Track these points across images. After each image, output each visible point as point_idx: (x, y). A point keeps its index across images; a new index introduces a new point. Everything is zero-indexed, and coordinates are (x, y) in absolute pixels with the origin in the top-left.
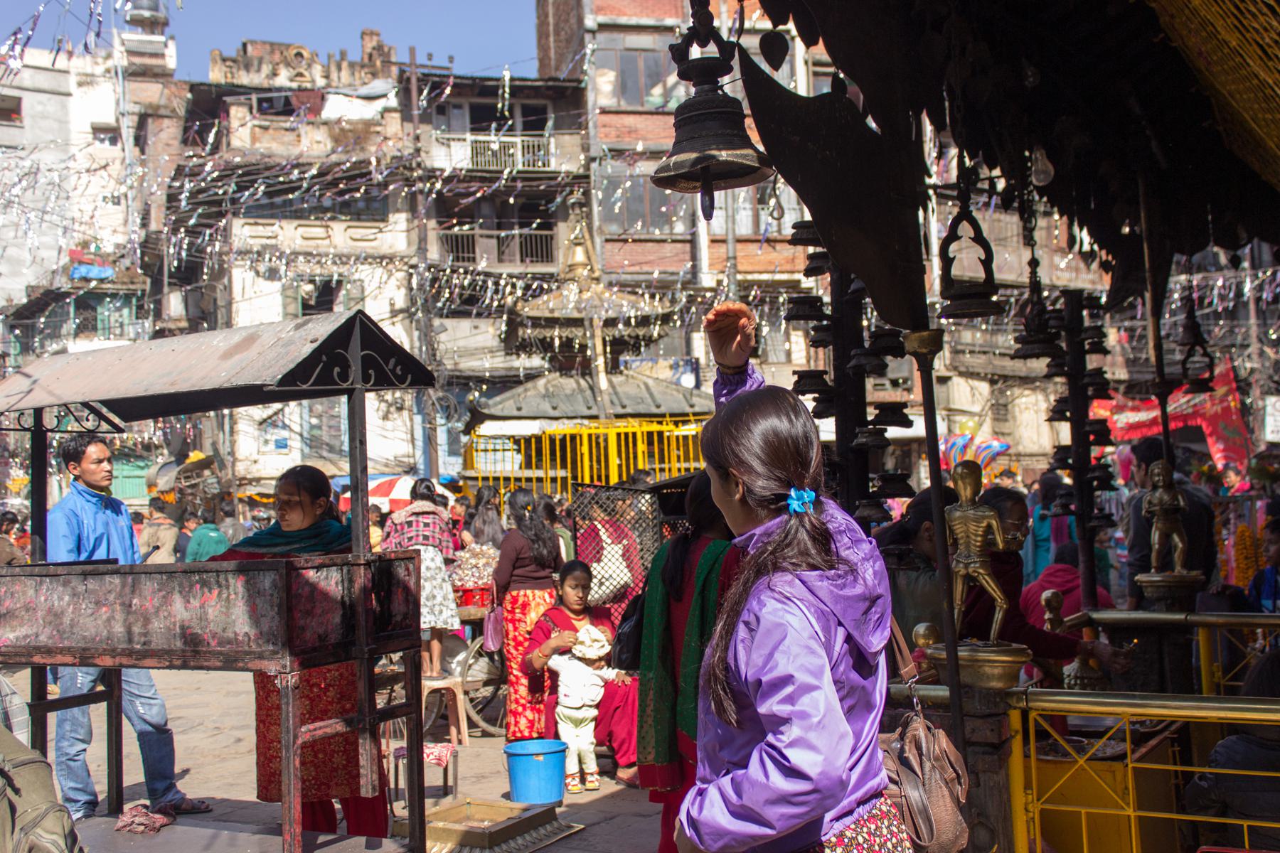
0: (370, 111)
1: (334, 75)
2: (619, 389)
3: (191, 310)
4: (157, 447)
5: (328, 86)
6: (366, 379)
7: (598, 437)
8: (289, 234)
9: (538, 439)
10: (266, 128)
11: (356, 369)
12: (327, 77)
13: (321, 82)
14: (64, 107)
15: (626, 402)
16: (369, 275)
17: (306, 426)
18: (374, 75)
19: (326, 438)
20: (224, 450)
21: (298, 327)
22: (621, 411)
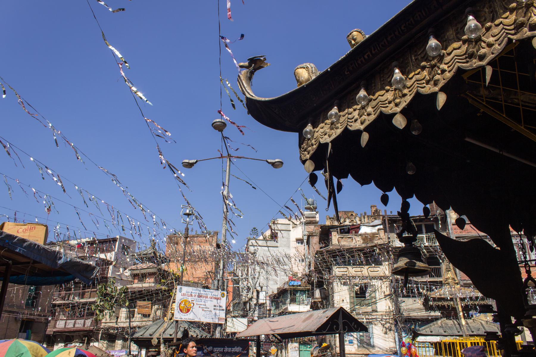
0: (375, 230)
1: (363, 220)
2: (470, 325)
3: (322, 296)
4: (314, 341)
5: (361, 223)
6: (344, 329)
7: (463, 343)
8: (352, 271)
9: (440, 343)
10: (343, 238)
11: (341, 326)
12: (360, 221)
13: (359, 222)
14: (289, 234)
15: (473, 330)
16: (376, 283)
17: (358, 336)
18: (375, 219)
19: (365, 340)
20: (333, 343)
21: (324, 312)
22: (472, 334)
